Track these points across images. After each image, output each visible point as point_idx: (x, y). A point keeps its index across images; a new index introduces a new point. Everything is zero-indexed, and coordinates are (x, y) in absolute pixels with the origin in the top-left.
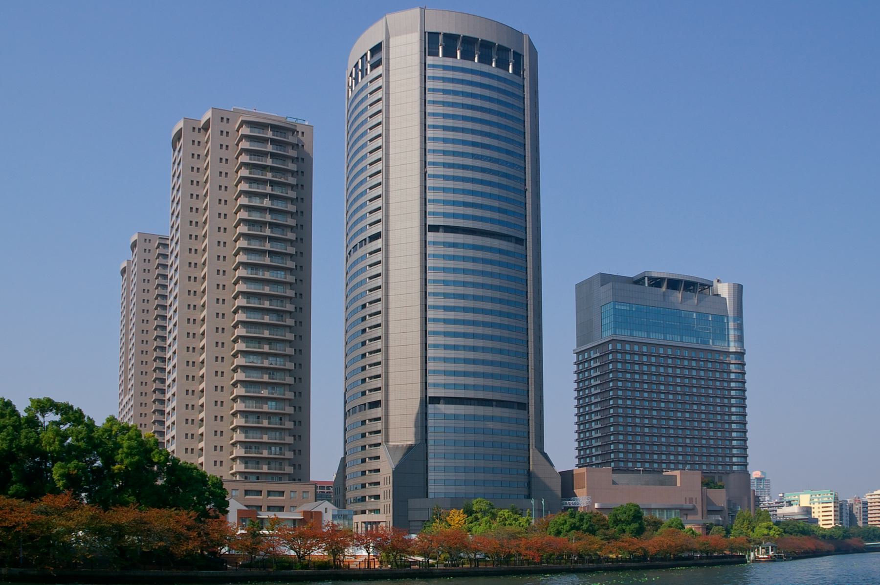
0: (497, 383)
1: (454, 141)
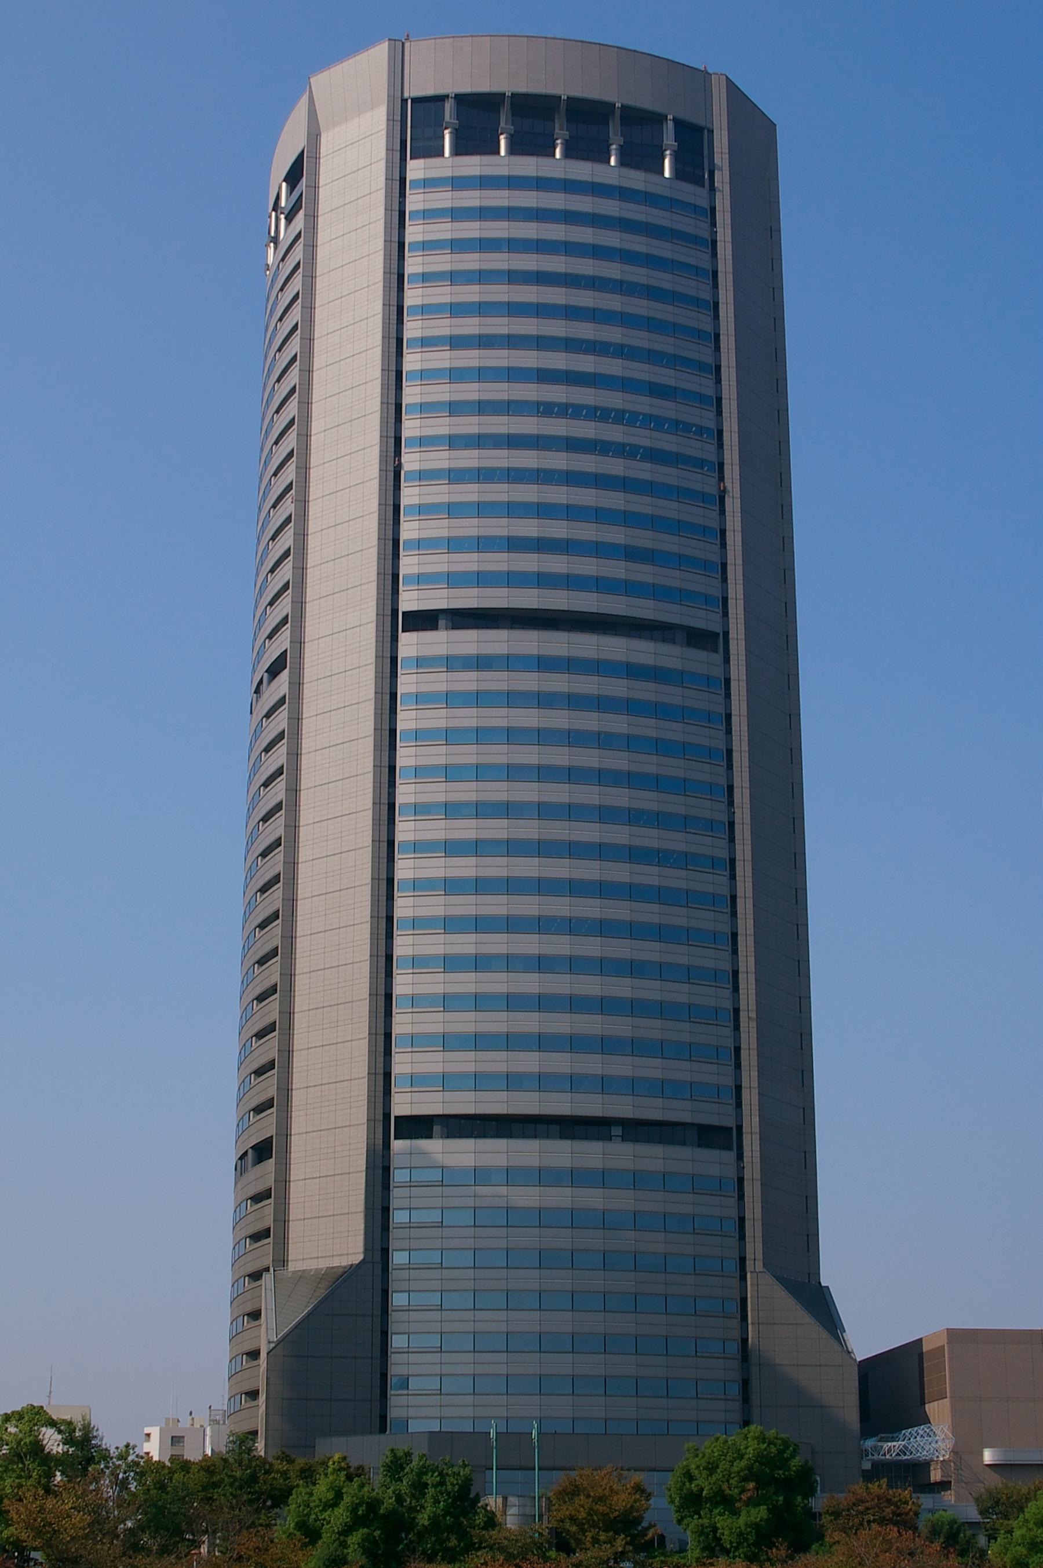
0: (622, 1066)
1: (482, 374)
